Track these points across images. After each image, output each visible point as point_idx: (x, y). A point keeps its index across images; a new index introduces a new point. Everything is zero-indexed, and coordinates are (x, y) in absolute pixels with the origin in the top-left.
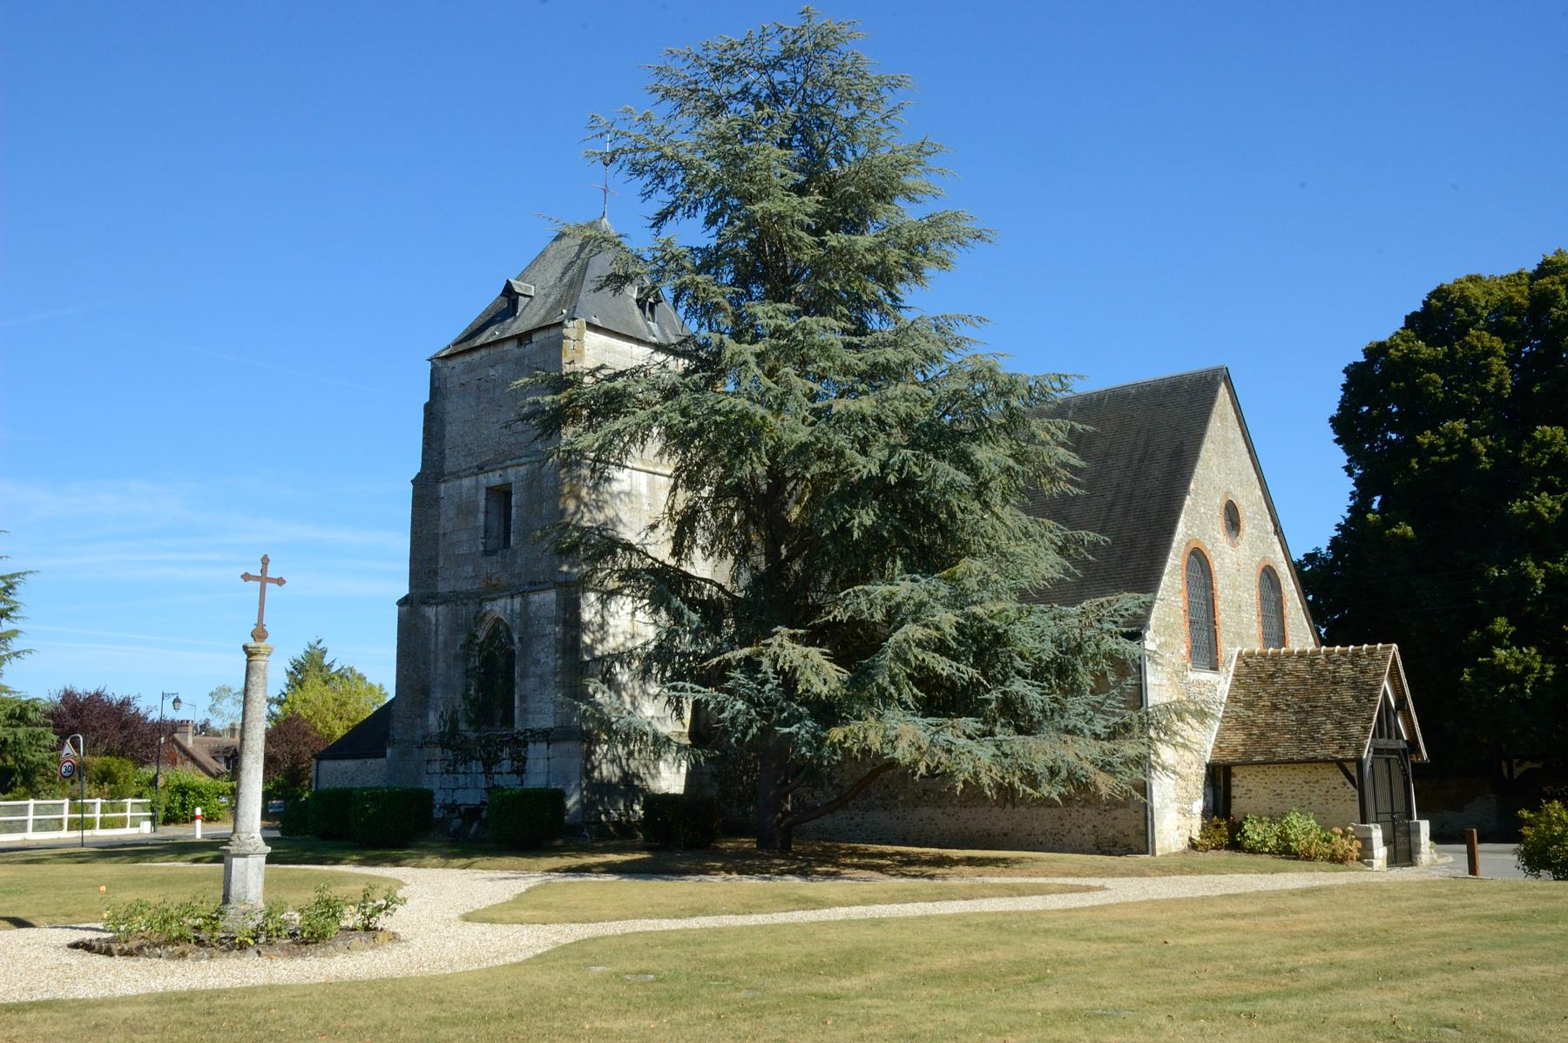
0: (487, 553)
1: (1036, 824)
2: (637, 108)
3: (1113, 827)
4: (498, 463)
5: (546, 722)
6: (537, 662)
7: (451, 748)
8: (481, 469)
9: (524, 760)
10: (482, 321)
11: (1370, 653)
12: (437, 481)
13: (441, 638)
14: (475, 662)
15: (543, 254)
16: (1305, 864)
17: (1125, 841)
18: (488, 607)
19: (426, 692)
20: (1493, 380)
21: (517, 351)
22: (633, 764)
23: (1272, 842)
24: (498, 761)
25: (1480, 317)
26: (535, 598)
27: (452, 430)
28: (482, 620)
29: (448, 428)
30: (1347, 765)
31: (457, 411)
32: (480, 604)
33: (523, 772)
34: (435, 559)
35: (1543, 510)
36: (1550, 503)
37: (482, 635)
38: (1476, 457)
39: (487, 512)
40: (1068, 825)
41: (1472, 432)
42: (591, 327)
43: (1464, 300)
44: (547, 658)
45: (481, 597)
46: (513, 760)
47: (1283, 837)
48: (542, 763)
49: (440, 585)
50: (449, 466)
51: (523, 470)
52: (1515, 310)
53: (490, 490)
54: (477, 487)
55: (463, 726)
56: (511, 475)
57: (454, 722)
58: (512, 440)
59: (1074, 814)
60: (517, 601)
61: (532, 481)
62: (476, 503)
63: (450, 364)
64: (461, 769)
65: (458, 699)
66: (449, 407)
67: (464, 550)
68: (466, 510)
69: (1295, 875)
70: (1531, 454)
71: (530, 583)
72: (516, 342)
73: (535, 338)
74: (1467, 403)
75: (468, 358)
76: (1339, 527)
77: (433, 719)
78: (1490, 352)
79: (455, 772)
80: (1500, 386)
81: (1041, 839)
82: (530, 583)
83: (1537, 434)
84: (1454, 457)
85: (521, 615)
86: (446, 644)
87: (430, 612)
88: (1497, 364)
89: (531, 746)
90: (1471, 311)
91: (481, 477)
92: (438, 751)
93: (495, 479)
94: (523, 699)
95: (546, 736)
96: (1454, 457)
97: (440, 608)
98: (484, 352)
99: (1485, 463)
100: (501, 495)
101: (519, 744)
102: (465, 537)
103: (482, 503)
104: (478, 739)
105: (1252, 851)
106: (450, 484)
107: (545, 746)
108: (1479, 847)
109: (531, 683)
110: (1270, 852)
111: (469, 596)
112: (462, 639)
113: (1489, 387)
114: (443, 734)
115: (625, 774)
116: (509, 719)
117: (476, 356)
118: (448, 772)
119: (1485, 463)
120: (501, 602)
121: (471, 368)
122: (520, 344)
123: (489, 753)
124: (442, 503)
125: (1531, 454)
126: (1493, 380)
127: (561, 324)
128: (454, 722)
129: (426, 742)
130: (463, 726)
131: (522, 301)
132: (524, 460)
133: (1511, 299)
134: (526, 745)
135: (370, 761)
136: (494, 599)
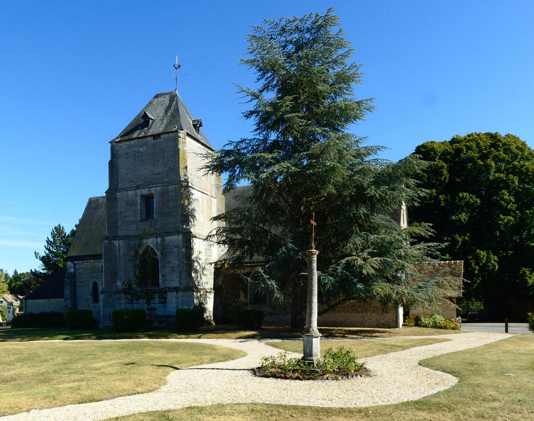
0: (141, 221)
1: (354, 319)
2: (243, 49)
3: (383, 319)
4: (147, 184)
5: (176, 284)
6: (170, 262)
7: (129, 294)
8: (138, 187)
9: (166, 298)
10: (130, 128)
11: (455, 263)
12: (116, 191)
13: (122, 253)
14: (138, 262)
15: (150, 103)
16: (444, 330)
17: (388, 324)
18: (145, 241)
19: (116, 274)
20: (444, 177)
21: (153, 141)
22: (202, 299)
23: (431, 324)
24: (153, 299)
25: (438, 155)
26: (168, 238)
27: (122, 172)
28: (142, 246)
29: (120, 170)
30: (453, 299)
31: (123, 164)
32: (141, 239)
33: (165, 302)
34: (116, 222)
35: (462, 219)
36: (464, 217)
37: (141, 252)
38: (440, 201)
39: (141, 205)
40: (366, 319)
41: (438, 194)
42: (188, 135)
43: (433, 149)
44: (174, 261)
45: (141, 237)
46: (160, 298)
47: (435, 322)
48: (174, 300)
49: (119, 232)
50: (121, 185)
51: (159, 189)
52: (449, 153)
53: (142, 196)
54: (136, 195)
55: (134, 286)
56: (153, 190)
57: (130, 285)
58: (152, 177)
59: (369, 315)
60: (159, 240)
61: (163, 194)
62: (136, 202)
63: (119, 144)
64: (135, 302)
65: (132, 276)
66: (120, 162)
67: (131, 219)
68: (131, 203)
69: (208, 343)
70: (460, 201)
71: (165, 233)
72: (152, 138)
73: (162, 136)
74: (435, 184)
75: (128, 143)
76: (76, 226)
77: (119, 283)
78: (442, 167)
79: (132, 303)
80: (445, 178)
81: (356, 323)
82: (165, 233)
83: (461, 195)
84: (432, 201)
85: (161, 245)
86: (124, 255)
87: (116, 243)
88: (445, 172)
89: (169, 293)
90: (435, 153)
91: (138, 191)
92: (123, 295)
93: (145, 192)
94: (163, 276)
95: (176, 289)
96: (432, 201)
97: (121, 241)
98: (136, 141)
99: (443, 204)
100: (148, 199)
101: (163, 293)
102: (131, 214)
103: (139, 201)
104: (142, 291)
105: (424, 326)
106: (121, 193)
107: (175, 293)
108: (509, 324)
109: (167, 270)
110: (431, 327)
111: (135, 237)
112: (132, 253)
113: (442, 179)
114: (125, 289)
115: (200, 302)
116: (156, 282)
117: (132, 142)
118: (128, 303)
119: (443, 204)
120: (151, 240)
121: (130, 147)
122: (154, 139)
123: (148, 296)
124: (118, 200)
125: (460, 201)
126: (444, 177)
127: (176, 131)
128: (130, 285)
129: (118, 292)
130: (134, 286)
131: (151, 121)
132: (159, 185)
133: (447, 150)
134: (166, 292)
135: (51, 300)
136: (147, 238)
